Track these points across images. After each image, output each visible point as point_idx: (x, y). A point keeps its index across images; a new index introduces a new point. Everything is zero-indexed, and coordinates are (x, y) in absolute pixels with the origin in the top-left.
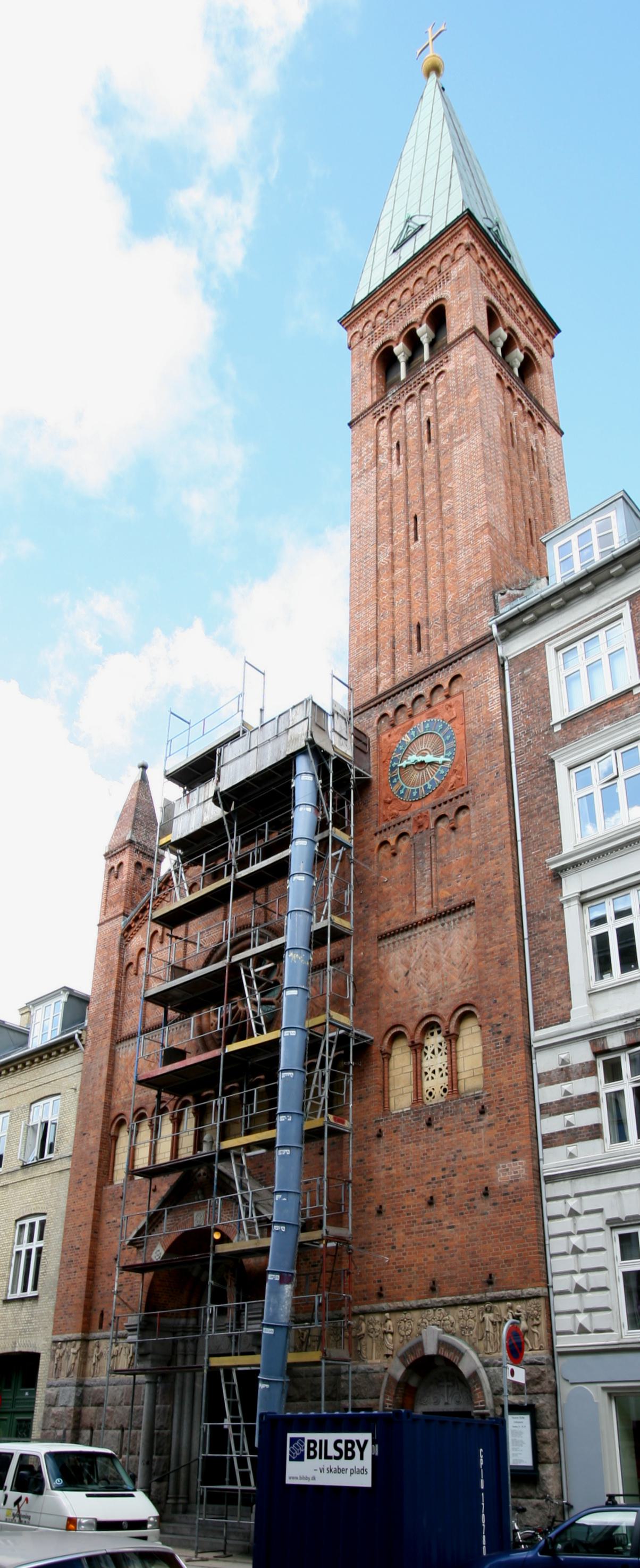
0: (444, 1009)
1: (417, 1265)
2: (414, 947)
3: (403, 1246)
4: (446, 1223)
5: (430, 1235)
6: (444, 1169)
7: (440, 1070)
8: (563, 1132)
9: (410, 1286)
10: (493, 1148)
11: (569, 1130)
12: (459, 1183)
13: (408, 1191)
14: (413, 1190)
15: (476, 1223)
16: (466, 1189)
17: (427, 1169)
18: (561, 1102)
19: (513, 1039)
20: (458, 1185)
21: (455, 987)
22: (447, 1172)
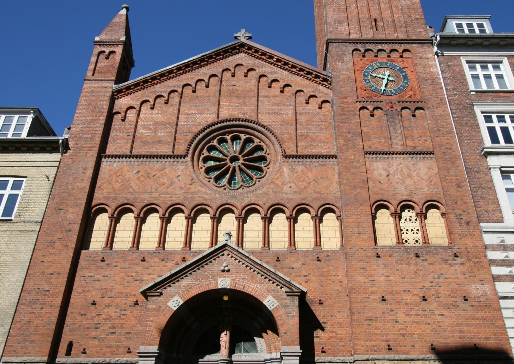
0: (419, 198)
1: (418, 334)
2: (391, 164)
3: (405, 322)
4: (437, 312)
5: (426, 317)
6: (431, 282)
7: (412, 230)
8: (507, 275)
9: (413, 346)
10: (465, 276)
11: (510, 275)
12: (443, 291)
13: (404, 291)
14: (409, 291)
15: (460, 315)
16: (449, 295)
17: (418, 280)
18: (503, 260)
19: (471, 223)
20: (443, 292)
21: (424, 190)
22: (434, 284)
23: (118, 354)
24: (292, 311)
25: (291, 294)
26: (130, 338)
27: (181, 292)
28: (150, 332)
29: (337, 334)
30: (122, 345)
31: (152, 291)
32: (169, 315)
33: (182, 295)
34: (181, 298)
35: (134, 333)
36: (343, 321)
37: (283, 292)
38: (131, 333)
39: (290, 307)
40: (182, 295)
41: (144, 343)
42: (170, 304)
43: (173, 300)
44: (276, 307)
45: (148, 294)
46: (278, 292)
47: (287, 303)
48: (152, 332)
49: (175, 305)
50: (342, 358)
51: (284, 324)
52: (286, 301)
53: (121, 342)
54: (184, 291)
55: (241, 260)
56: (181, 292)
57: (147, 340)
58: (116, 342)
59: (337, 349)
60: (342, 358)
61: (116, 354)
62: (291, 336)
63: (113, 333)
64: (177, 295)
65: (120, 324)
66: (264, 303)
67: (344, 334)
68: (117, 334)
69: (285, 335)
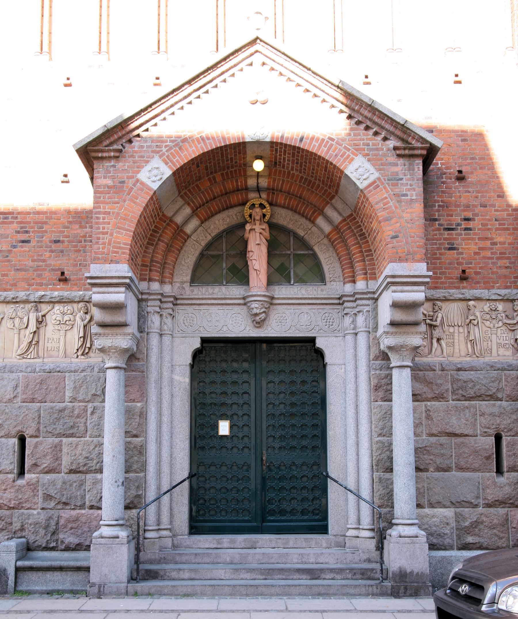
23: (41, 284)
24: (409, 190)
25: (407, 152)
26: (62, 252)
27: (164, 150)
28: (108, 236)
29: (495, 244)
30: (46, 265)
31: (100, 147)
32: (143, 200)
33: (168, 157)
34: (166, 163)
35: (69, 242)
36: (508, 215)
37: (388, 150)
38: (63, 242)
39: (404, 181)
40: (168, 157)
41: (98, 258)
42: (143, 176)
43: (148, 167)
44: (374, 182)
45: (93, 154)
46: (377, 149)
47: (397, 174)
48: (112, 235)
49: (154, 179)
50: (503, 292)
51: (391, 218)
52: (395, 169)
53: (44, 261)
54: (171, 148)
55: (293, 77)
56: (164, 150)
57: (103, 253)
58: (33, 261)
59: (493, 273)
60: (503, 292)
61: (37, 284)
62: (407, 243)
63: (23, 242)
64: (157, 157)
65: (35, 223)
66: (347, 172)
67: (510, 244)
68: (32, 244)
69: (394, 240)
